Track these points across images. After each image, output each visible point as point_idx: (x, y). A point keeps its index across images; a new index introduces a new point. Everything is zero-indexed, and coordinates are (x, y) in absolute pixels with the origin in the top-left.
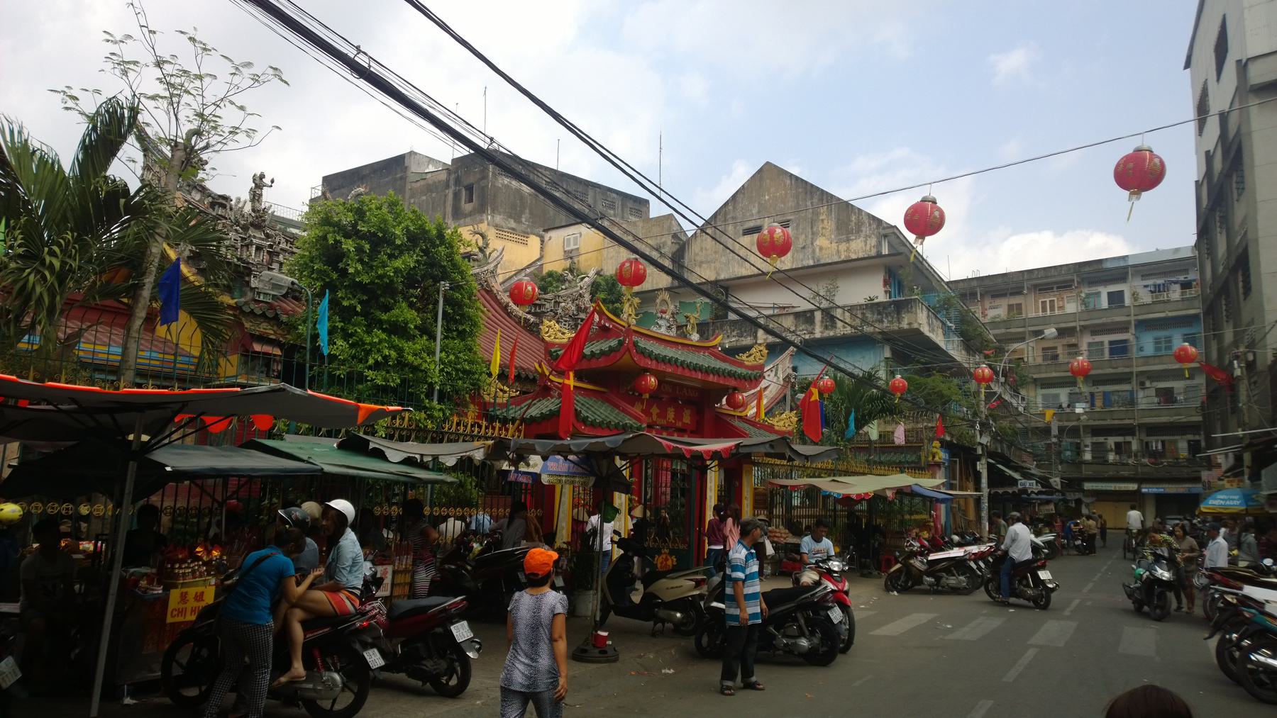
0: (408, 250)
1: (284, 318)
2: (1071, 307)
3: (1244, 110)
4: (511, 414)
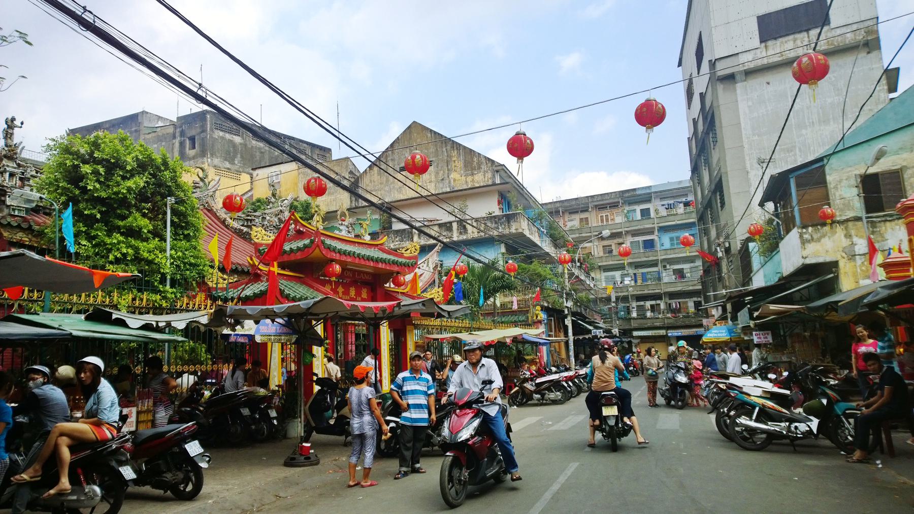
0: (139, 173)
1: (36, 228)
2: (619, 219)
3: (714, 91)
4: (230, 295)
